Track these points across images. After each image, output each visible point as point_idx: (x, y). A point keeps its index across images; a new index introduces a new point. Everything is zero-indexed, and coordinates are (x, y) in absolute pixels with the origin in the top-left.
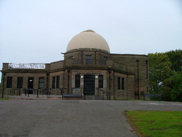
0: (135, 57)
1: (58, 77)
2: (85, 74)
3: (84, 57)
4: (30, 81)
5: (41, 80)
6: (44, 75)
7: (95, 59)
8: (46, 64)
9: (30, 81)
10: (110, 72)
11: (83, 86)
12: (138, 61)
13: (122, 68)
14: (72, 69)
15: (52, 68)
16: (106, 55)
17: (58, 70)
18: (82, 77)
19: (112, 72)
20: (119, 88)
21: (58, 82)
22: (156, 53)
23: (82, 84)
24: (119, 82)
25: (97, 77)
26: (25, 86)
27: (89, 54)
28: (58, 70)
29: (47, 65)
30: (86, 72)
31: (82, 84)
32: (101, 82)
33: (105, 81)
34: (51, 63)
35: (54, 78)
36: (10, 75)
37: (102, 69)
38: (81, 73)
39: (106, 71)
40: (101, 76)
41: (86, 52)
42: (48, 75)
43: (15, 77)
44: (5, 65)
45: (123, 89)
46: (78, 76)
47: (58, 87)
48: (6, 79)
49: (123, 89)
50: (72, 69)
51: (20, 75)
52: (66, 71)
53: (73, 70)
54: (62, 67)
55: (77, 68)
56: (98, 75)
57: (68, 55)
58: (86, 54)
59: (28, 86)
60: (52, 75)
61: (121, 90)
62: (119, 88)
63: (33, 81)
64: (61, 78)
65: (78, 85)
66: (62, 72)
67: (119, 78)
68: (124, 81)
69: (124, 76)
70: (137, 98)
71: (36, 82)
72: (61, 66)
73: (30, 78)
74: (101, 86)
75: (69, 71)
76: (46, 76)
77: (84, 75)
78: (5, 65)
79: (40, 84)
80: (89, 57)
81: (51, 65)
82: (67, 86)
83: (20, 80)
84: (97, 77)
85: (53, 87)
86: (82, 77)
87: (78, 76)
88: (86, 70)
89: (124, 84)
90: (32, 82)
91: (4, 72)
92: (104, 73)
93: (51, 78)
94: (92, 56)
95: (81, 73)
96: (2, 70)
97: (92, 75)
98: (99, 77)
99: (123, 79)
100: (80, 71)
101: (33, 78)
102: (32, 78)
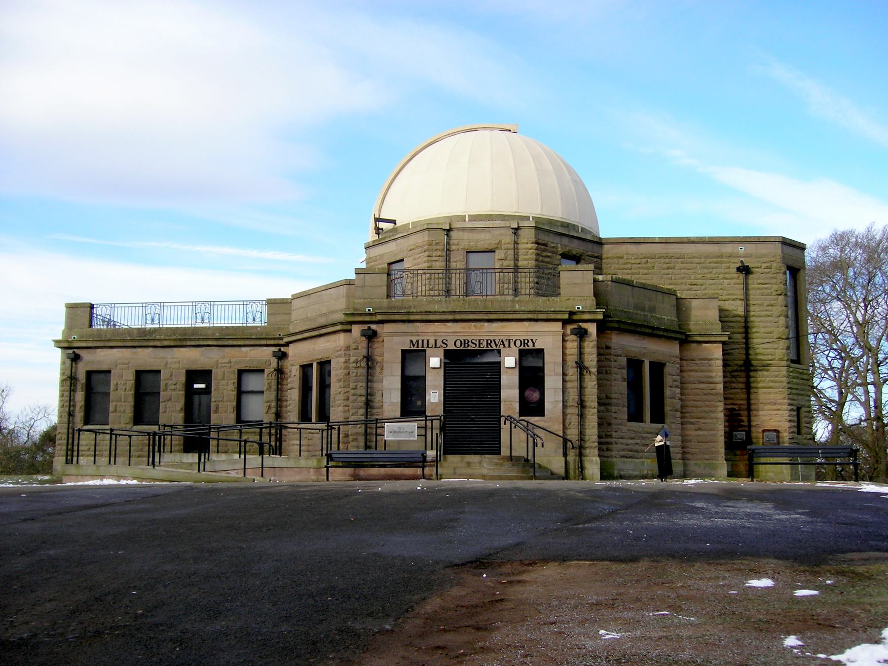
0: (728, 249)
1: (324, 365)
2: (451, 347)
3: (457, 261)
4: (196, 386)
7: (516, 269)
8: (271, 303)
9: (196, 386)
11: (440, 411)
12: (745, 270)
13: (652, 309)
14: (287, 344)
15: (298, 320)
16: (576, 247)
17: (318, 332)
20: (635, 416)
21: (324, 386)
23: (434, 397)
24: (635, 385)
26: (171, 410)
27: (481, 246)
28: (318, 332)
29: (273, 304)
30: (454, 335)
31: (434, 397)
33: (552, 382)
34: (296, 297)
35: (306, 369)
38: (432, 343)
41: (466, 236)
43: (122, 364)
44: (82, 313)
45: (658, 416)
46: (412, 356)
47: (323, 416)
49: (658, 416)
51: (146, 358)
54: (340, 317)
56: (515, 350)
58: (464, 245)
61: (647, 425)
62: (635, 416)
65: (411, 403)
66: (341, 340)
67: (635, 365)
69: (666, 350)
70: (742, 467)
71: (223, 390)
72: (337, 308)
73: (193, 376)
74: (532, 407)
75: (371, 336)
76: (274, 362)
77: (448, 354)
78: (82, 313)
79: (245, 399)
80: (476, 261)
81: (294, 302)
82: (362, 411)
83: (145, 385)
85: (305, 416)
86: (435, 362)
87: (412, 356)
90: (207, 391)
91: (72, 352)
92: (548, 337)
94: (499, 254)
95: (432, 343)
96: (60, 338)
97: (482, 352)
99: (658, 368)
101: (210, 372)
102: (205, 375)
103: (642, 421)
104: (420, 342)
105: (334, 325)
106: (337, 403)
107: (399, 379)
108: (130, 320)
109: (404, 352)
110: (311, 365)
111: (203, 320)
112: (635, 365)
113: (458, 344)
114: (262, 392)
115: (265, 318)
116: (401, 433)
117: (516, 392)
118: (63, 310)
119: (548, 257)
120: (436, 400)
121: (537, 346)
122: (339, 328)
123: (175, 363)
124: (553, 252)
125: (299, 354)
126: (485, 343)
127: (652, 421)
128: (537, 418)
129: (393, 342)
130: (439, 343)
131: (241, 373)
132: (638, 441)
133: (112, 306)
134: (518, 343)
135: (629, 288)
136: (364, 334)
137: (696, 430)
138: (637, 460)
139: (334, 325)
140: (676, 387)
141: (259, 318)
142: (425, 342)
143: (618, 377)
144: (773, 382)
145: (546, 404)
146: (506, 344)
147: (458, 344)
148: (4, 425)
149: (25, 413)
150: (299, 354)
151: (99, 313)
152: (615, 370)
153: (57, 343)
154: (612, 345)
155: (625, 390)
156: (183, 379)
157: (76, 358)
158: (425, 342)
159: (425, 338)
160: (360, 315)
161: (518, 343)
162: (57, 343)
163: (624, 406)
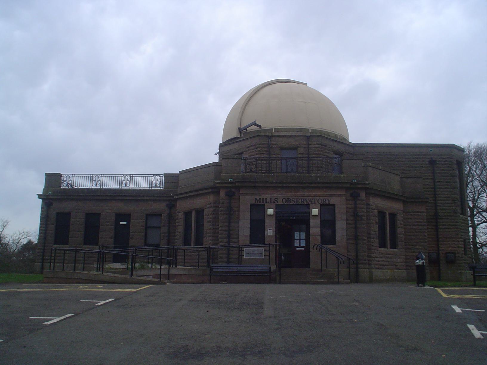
1: (200, 212)
2: (280, 202)
4: (121, 223)
11: (273, 241)
23: (270, 232)
26: (106, 236)
29: (168, 177)
31: (270, 232)
33: (341, 226)
35: (188, 214)
38: (268, 200)
46: (258, 208)
62: (383, 245)
65: (257, 236)
67: (381, 214)
73: (120, 217)
75: (230, 195)
83: (92, 223)
85: (187, 242)
90: (127, 226)
95: (268, 200)
99: (393, 216)
102: (126, 217)
103: (385, 248)
104: (262, 199)
105: (206, 189)
106: (208, 235)
107: (249, 221)
108: (80, 184)
109: (251, 205)
110: (191, 212)
111: (96, 185)
112: (381, 214)
113: (284, 200)
114: (159, 228)
115: (162, 185)
116: (254, 254)
117: (319, 230)
118: (44, 178)
119: (327, 152)
120: (271, 234)
121: (331, 203)
122: (210, 190)
123: (108, 211)
124: (329, 150)
125: (182, 206)
126: (300, 201)
127: (390, 248)
128: (332, 246)
129: (246, 200)
130: (273, 200)
131: (147, 215)
132: (384, 259)
133: (73, 175)
134: (320, 201)
135: (378, 171)
136: (227, 194)
137: (412, 252)
138: (384, 271)
139: (206, 189)
140: (402, 227)
141: (160, 185)
142: (264, 199)
143: (373, 221)
144: (450, 225)
145: (337, 237)
146: (313, 201)
147: (284, 200)
148: (3, 241)
149: (15, 235)
150: (182, 206)
151: (65, 179)
152: (372, 218)
153: (40, 196)
154: (371, 203)
155: (377, 229)
156: (113, 218)
157: (51, 204)
158: (264, 199)
159: (264, 197)
160: (225, 183)
161: (320, 201)
162: (40, 196)
163: (376, 239)
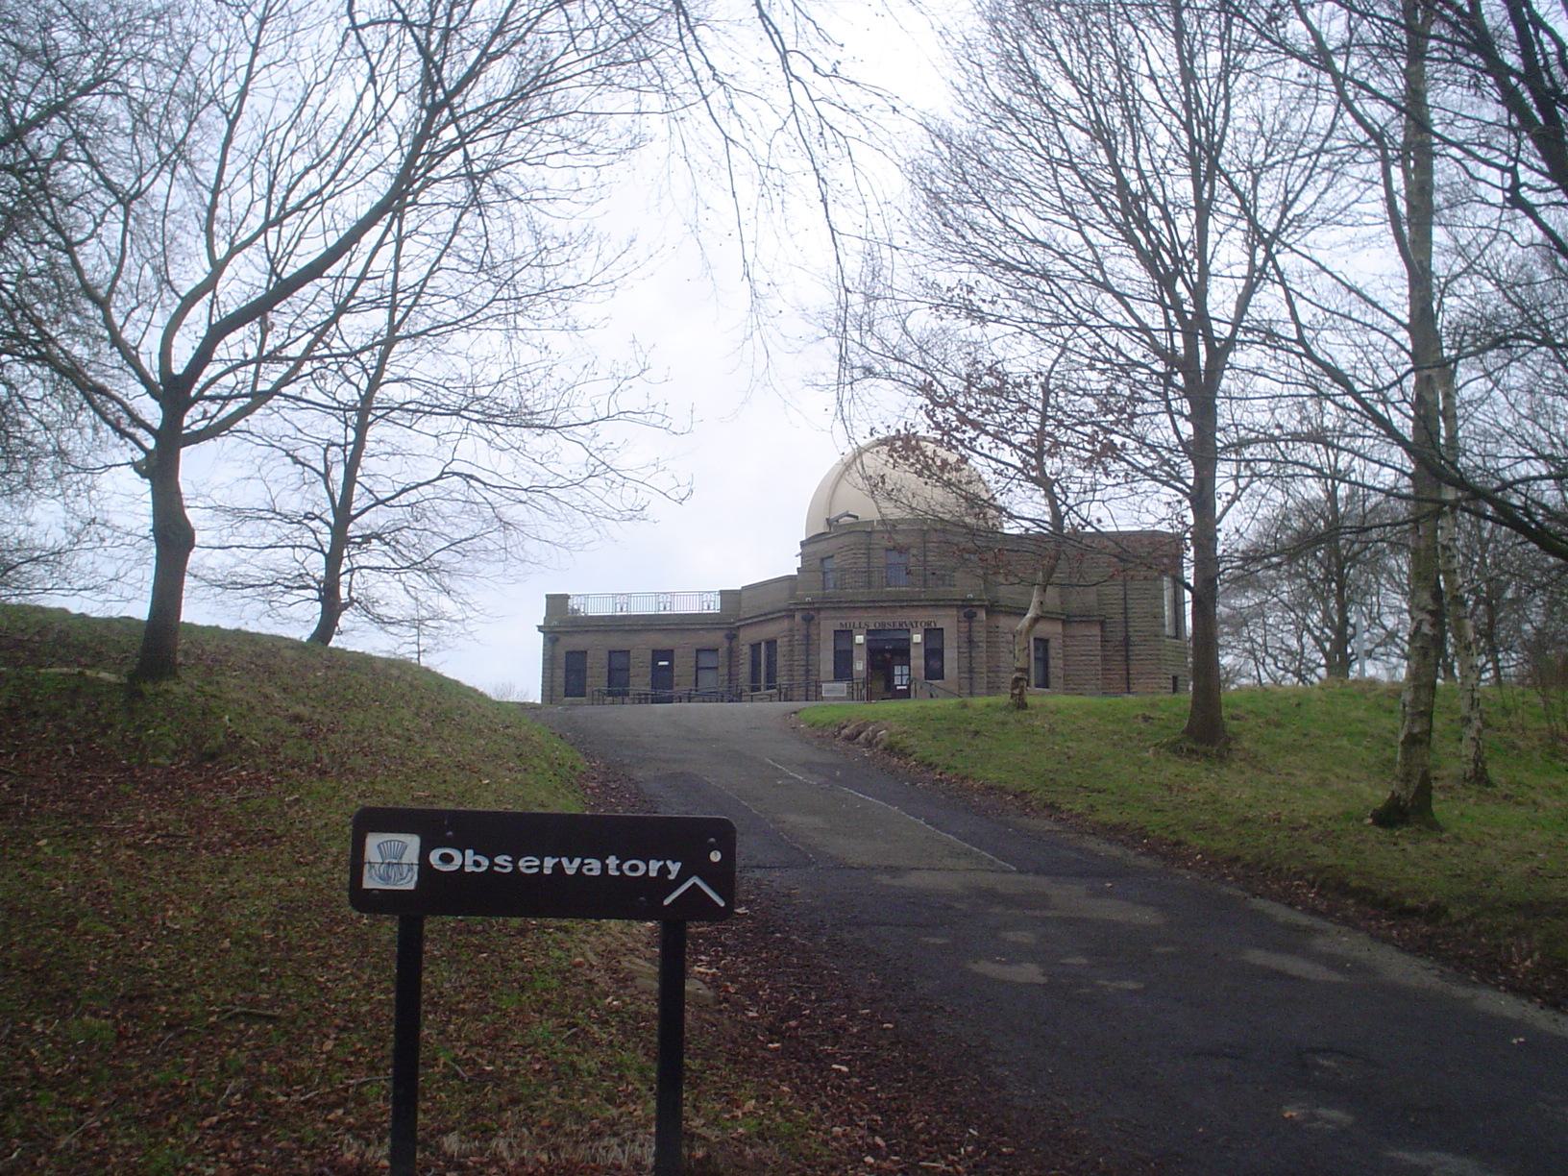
1: (771, 644)
4: (666, 902)
5: (706, 660)
6: (717, 638)
8: (722, 593)
10: (970, 617)
14: (819, 610)
17: (766, 618)
18: (860, 639)
19: (982, 615)
22: (540, 628)
23: (860, 666)
25: (917, 638)
32: (934, 653)
33: (950, 656)
34: (745, 588)
35: (755, 647)
36: (578, 642)
37: (937, 604)
39: (954, 612)
40: (933, 634)
42: (732, 637)
43: (598, 649)
44: (557, 603)
46: (844, 635)
48: (562, 661)
50: (819, 610)
52: (798, 616)
53: (823, 614)
55: (838, 606)
57: (836, 543)
59: (630, 918)
60: (747, 637)
63: (672, 662)
64: (782, 647)
66: (785, 624)
68: (1052, 652)
71: (683, 666)
75: (808, 620)
77: (869, 632)
84: (917, 638)
86: (860, 639)
88: (877, 613)
89: (1052, 663)
92: (948, 622)
93: (746, 649)
98: (925, 638)
100: (853, 619)
102: (668, 654)
